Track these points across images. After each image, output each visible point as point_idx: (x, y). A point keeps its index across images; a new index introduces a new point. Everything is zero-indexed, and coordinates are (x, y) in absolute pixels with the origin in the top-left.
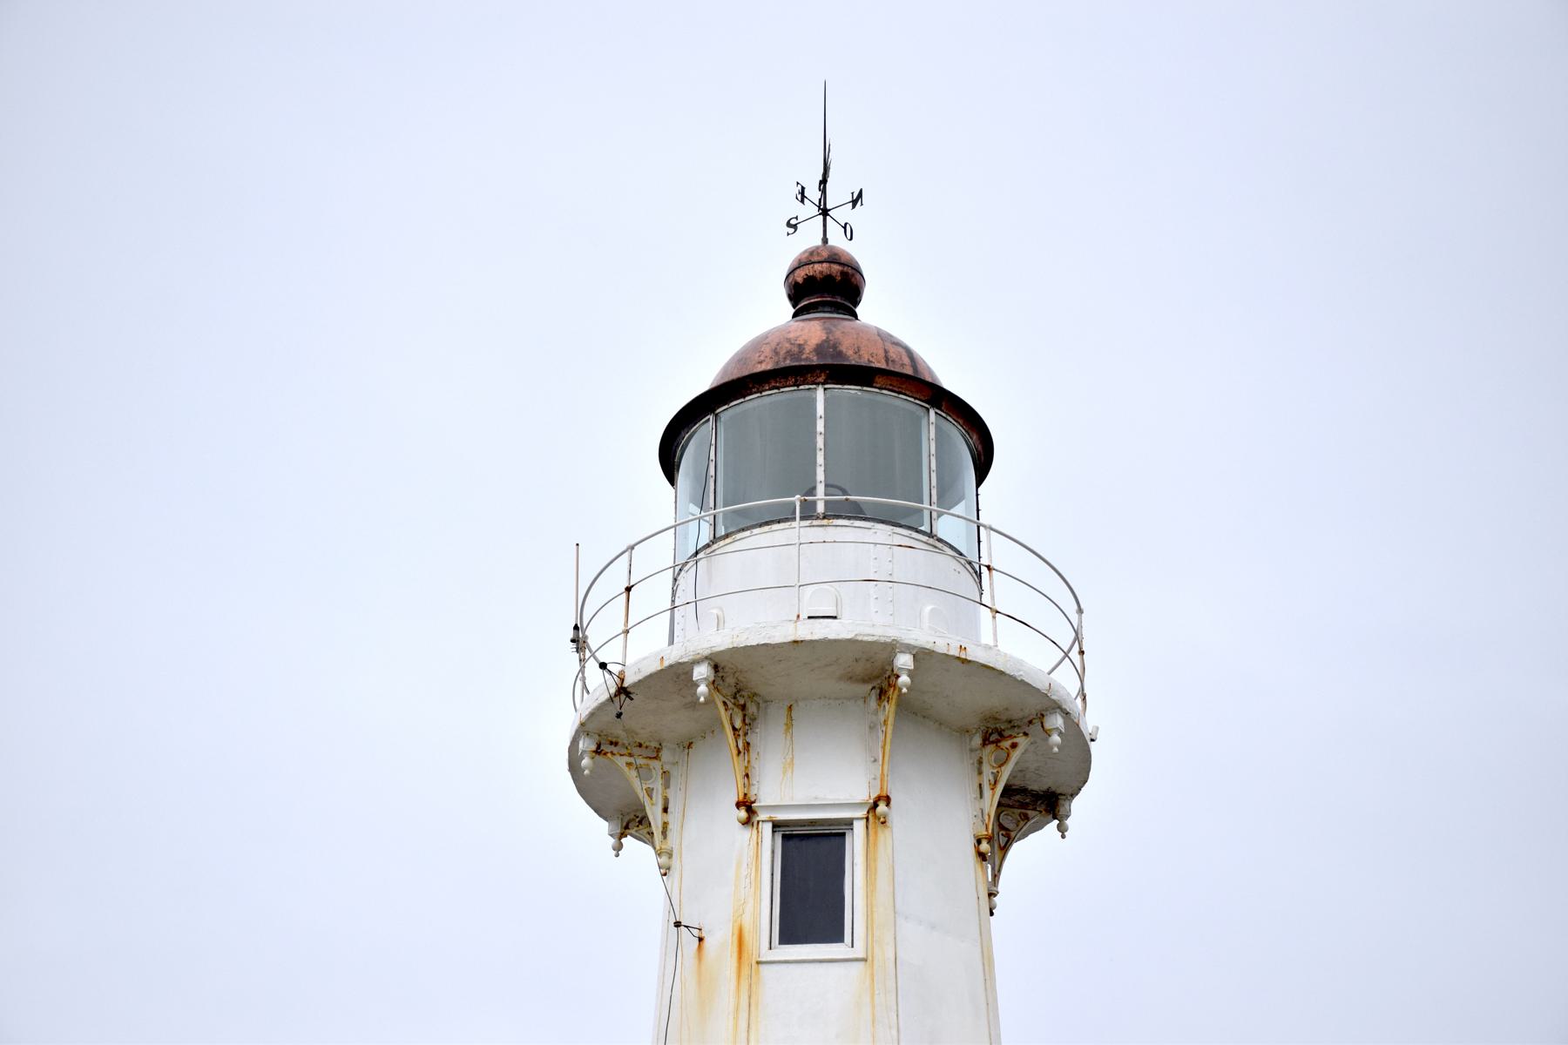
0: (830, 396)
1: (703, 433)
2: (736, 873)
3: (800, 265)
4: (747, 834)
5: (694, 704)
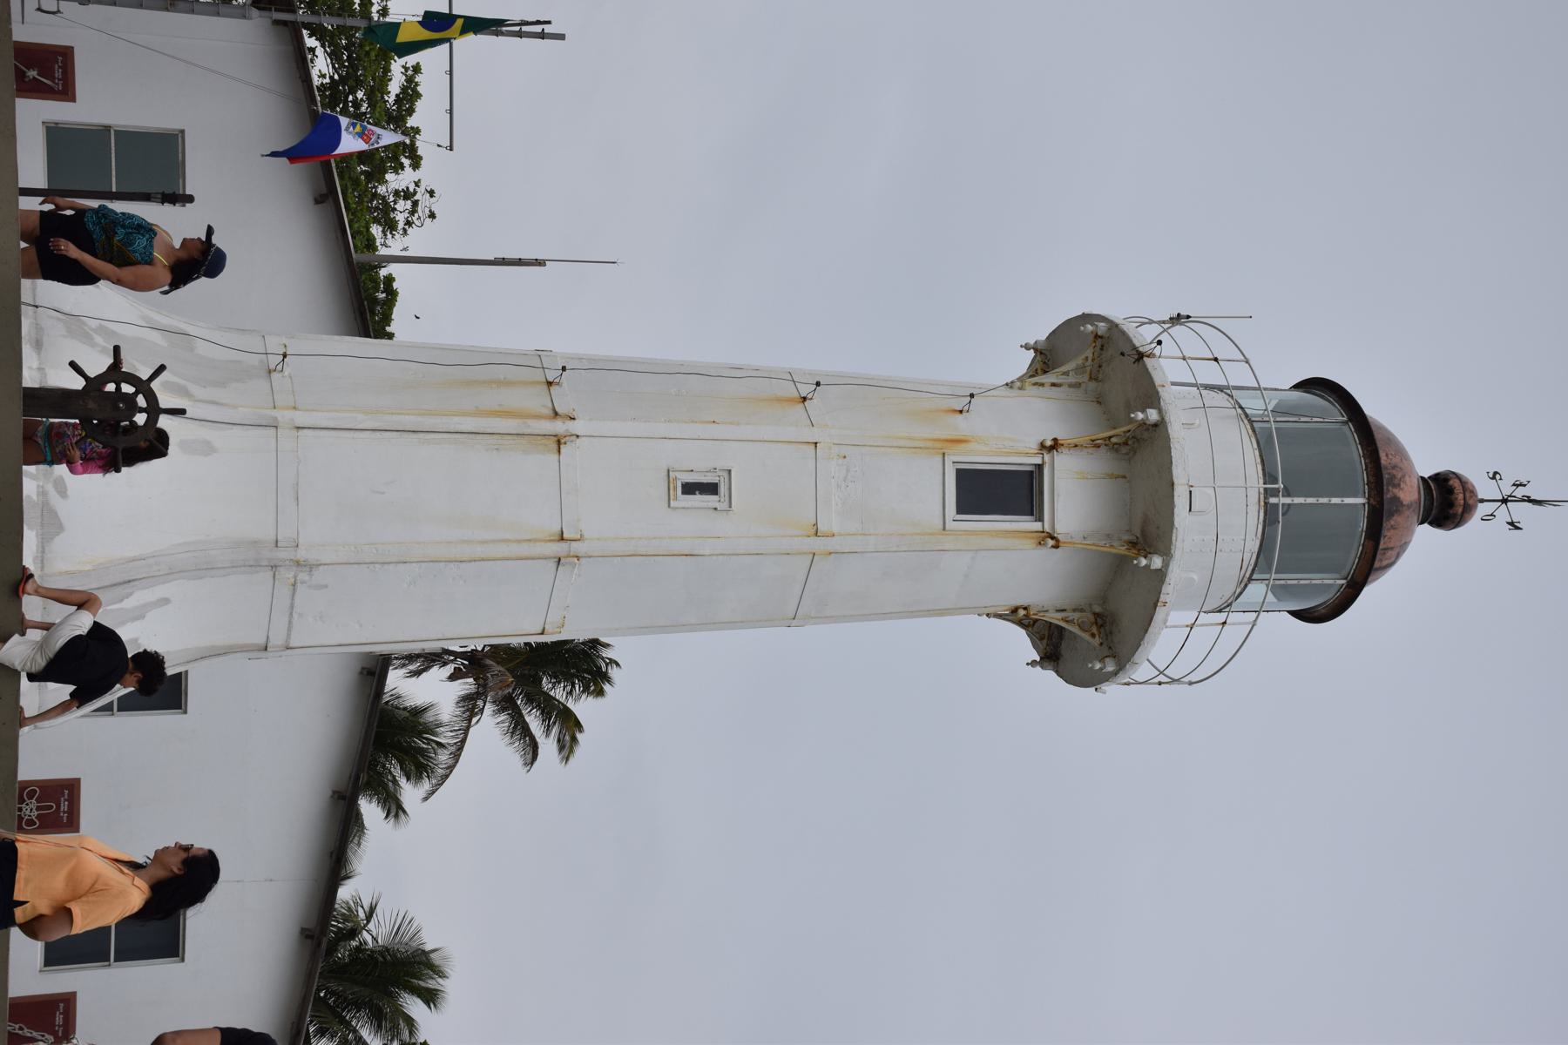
0: (1353, 502)
1: (1336, 414)
2: (1011, 433)
3: (1464, 483)
4: (1033, 445)
5: (1130, 408)
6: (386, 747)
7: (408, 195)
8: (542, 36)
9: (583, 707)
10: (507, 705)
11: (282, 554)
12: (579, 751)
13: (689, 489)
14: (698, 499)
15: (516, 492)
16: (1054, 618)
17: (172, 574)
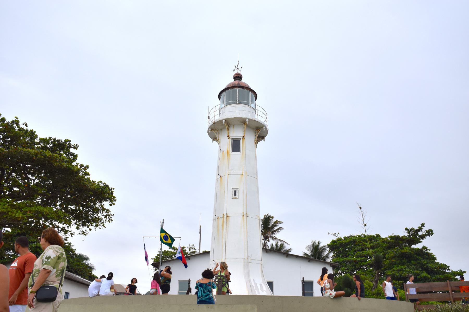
0: (238, 90)
1: (224, 94)
2: (227, 144)
3: (235, 75)
4: (229, 140)
5: (223, 125)
6: (280, 251)
7: (190, 249)
8: (163, 222)
9: (274, 220)
10: (273, 233)
11: (246, 261)
12: (281, 221)
13: (235, 195)
14: (237, 194)
15: (236, 223)
16: (257, 137)
17: (250, 282)
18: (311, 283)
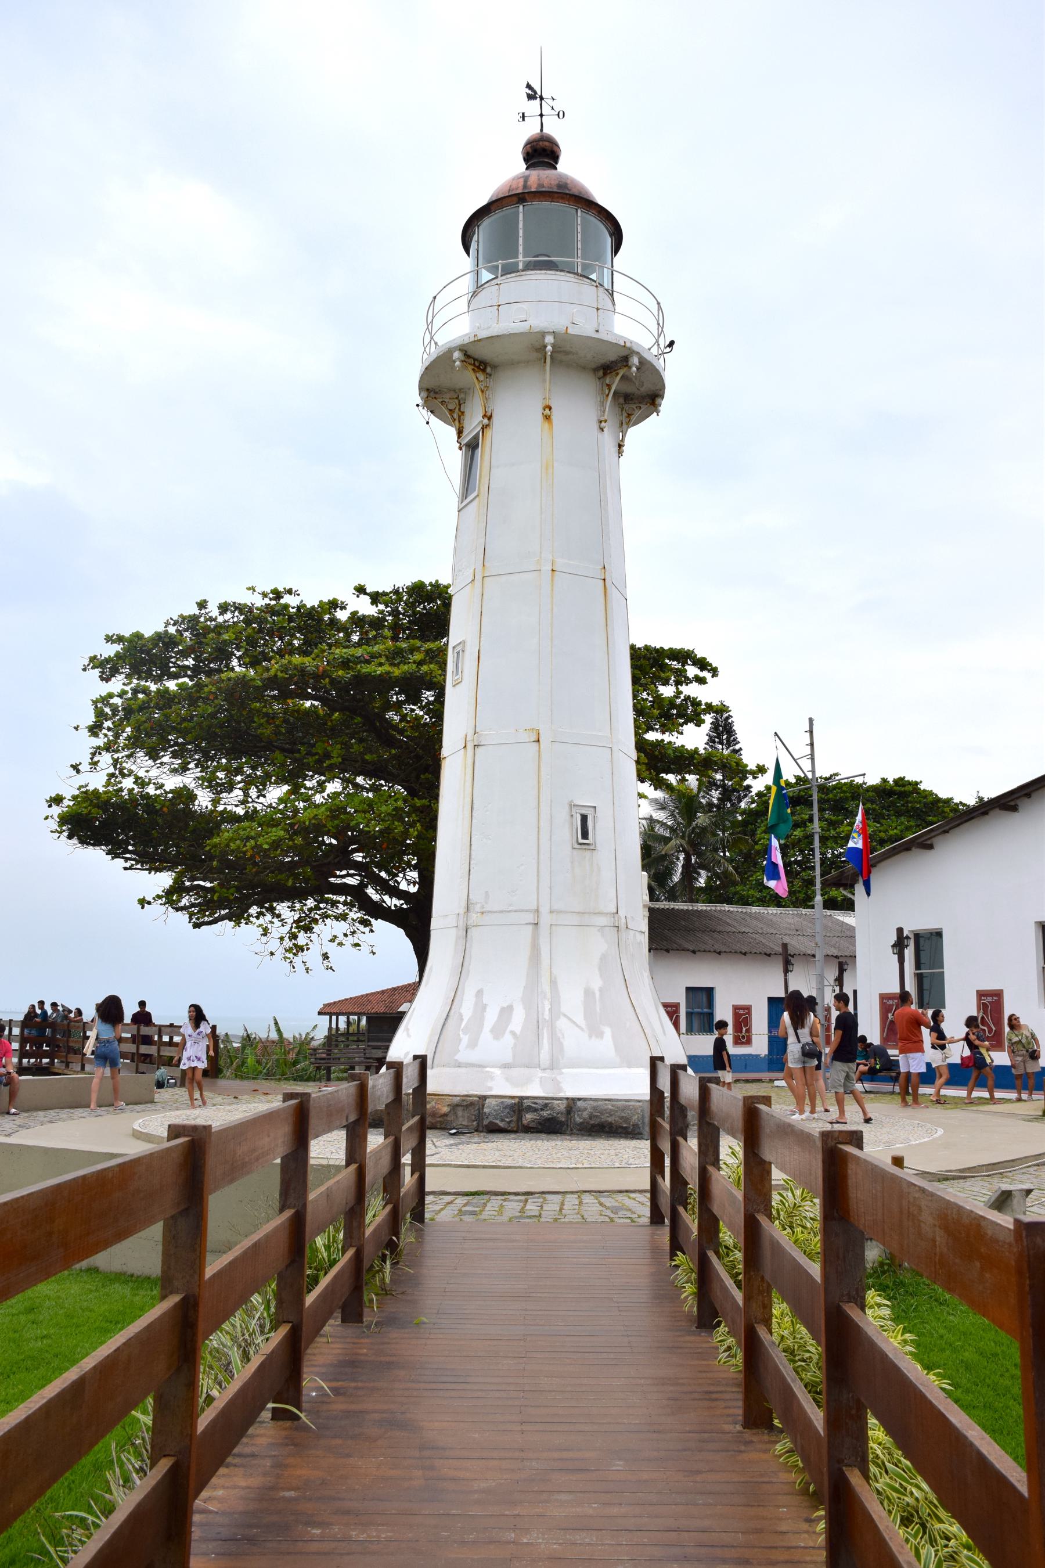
0: (542, 215)
1: (486, 223)
18: (748, 1009)
